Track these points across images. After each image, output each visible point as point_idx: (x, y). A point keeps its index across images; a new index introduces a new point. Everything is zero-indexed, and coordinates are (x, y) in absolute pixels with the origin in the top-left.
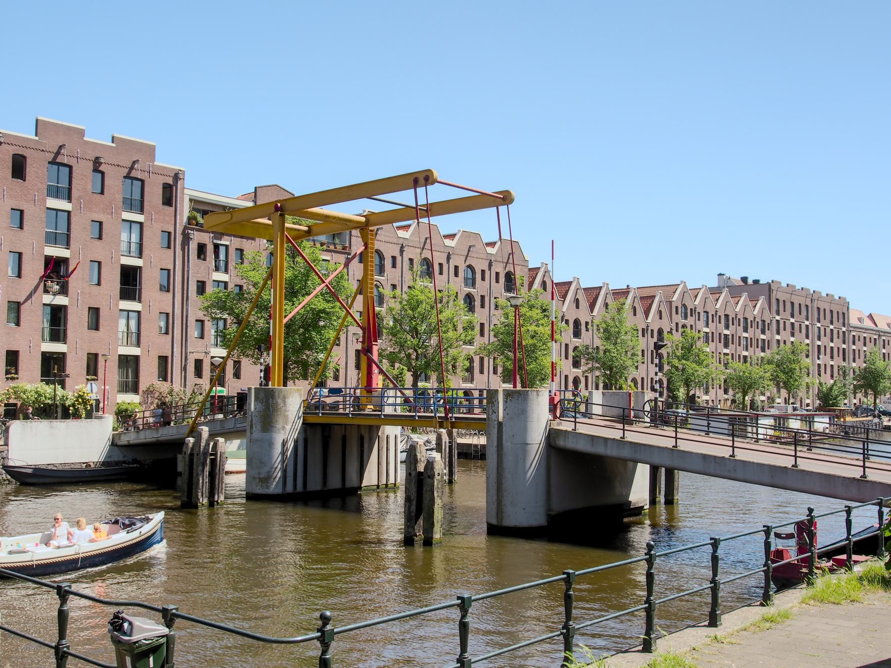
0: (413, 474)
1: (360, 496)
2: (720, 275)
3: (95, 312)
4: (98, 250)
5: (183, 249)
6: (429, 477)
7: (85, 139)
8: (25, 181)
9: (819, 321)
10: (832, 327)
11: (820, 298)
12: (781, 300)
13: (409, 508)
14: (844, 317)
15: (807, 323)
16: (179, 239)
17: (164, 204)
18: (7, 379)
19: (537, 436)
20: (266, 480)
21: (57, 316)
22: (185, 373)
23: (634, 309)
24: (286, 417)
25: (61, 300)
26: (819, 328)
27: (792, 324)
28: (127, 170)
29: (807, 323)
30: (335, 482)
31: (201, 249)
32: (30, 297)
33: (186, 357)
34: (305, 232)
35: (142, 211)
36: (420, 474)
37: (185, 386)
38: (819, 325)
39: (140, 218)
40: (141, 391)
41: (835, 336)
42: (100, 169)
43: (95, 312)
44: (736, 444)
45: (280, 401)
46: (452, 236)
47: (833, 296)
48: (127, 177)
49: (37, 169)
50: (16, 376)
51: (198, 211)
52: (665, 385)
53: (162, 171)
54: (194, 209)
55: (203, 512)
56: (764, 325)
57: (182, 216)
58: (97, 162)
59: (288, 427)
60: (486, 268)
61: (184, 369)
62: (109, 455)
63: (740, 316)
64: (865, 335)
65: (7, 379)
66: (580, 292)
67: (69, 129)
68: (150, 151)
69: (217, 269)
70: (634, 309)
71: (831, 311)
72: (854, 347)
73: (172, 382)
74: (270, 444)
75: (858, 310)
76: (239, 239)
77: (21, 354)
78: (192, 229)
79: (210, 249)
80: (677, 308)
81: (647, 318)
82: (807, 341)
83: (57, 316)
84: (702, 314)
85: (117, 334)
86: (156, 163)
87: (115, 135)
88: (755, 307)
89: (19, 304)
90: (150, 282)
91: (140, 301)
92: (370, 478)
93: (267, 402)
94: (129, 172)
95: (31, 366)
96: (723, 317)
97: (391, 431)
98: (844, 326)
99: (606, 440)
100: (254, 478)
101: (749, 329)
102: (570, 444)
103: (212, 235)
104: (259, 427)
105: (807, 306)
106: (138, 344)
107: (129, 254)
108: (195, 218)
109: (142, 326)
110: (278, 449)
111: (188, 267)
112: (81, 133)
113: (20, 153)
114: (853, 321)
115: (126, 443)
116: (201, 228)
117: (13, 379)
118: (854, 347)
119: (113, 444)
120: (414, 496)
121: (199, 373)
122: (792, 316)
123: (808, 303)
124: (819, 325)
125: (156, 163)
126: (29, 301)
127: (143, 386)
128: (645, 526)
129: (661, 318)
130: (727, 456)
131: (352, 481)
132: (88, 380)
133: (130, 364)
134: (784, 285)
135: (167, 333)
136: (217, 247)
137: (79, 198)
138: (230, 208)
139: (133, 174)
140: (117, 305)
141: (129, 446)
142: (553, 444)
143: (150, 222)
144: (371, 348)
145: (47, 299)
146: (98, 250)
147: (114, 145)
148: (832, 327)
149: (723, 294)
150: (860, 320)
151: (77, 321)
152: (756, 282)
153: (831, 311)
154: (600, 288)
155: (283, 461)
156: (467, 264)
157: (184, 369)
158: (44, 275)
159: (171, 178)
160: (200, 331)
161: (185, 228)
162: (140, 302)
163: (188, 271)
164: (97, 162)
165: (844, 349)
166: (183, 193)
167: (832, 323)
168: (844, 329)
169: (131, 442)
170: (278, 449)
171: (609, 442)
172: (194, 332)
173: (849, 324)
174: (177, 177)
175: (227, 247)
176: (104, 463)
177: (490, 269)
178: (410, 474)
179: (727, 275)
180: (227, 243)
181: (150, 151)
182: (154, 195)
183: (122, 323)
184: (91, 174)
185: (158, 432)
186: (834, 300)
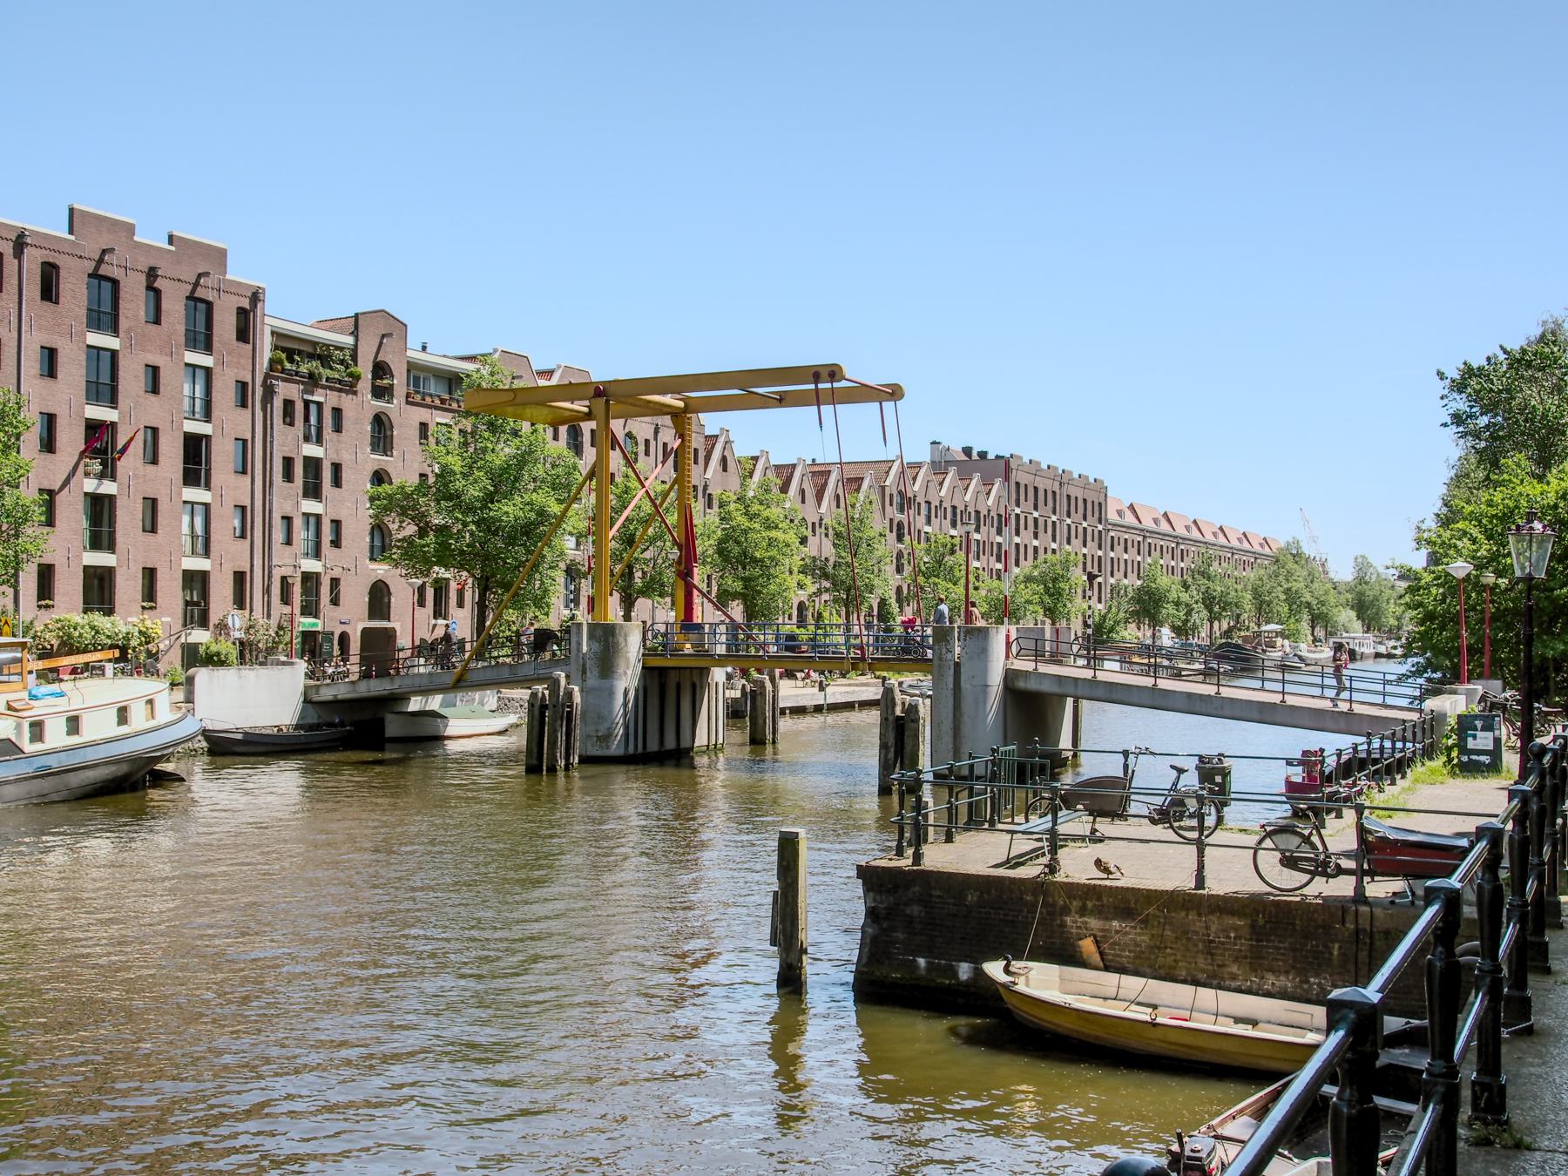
0: (891, 718)
1: (693, 758)
2: (934, 443)
3: (152, 504)
4: (153, 411)
5: (264, 409)
6: (913, 721)
7: (136, 238)
8: (57, 302)
9: (1069, 515)
10: (1085, 524)
11: (1070, 481)
12: (1022, 483)
13: (886, 756)
14: (1099, 509)
15: (1054, 518)
16: (259, 392)
17: (238, 339)
18: (40, 607)
19: (996, 678)
20: (606, 738)
21: (100, 510)
22: (269, 597)
23: (803, 492)
24: (627, 659)
25: (108, 488)
26: (1069, 526)
27: (1036, 520)
28: (190, 287)
29: (1054, 518)
30: (670, 744)
31: (288, 405)
32: (67, 482)
33: (270, 572)
34: (586, 414)
35: (115, 331)
36: (899, 718)
37: (269, 616)
38: (1069, 521)
39: (207, 361)
40: (211, 625)
41: (1089, 538)
42: (156, 285)
43: (152, 504)
44: (1222, 682)
45: (621, 640)
46: (550, 373)
47: (1039, 464)
48: (191, 298)
49: (74, 288)
50: (51, 603)
51: (284, 350)
52: (875, 613)
53: (235, 288)
54: (276, 348)
55: (561, 774)
56: (954, 514)
57: (262, 358)
58: (152, 274)
59: (629, 672)
60: (650, 436)
61: (267, 591)
62: (302, 717)
63: (971, 509)
64: (1126, 536)
65: (40, 607)
66: (771, 475)
67: (115, 223)
68: (220, 256)
69: (307, 439)
70: (803, 492)
71: (1036, 489)
72: (1112, 554)
73: (251, 611)
74: (611, 693)
75: (1119, 497)
76: (336, 393)
77: (57, 568)
78: (277, 378)
79: (299, 407)
80: (891, 495)
81: (819, 505)
82: (1054, 546)
83: (100, 510)
84: (923, 506)
85: (180, 538)
86: (228, 277)
87: (76, 206)
88: (967, 489)
89: (51, 493)
90: (222, 457)
91: (208, 486)
92: (701, 739)
93: (606, 641)
94: (97, 268)
95: (69, 587)
96: (949, 510)
97: (718, 675)
98: (1100, 523)
99: (1076, 679)
100: (589, 736)
101: (982, 528)
102: (1032, 685)
103: (301, 387)
104: (596, 673)
105: (1054, 493)
106: (207, 553)
107: (192, 416)
108: (280, 362)
109: (213, 525)
110: (619, 700)
111: (272, 436)
112: (130, 229)
113: (51, 260)
114: (1112, 516)
115: (331, 698)
116: (290, 377)
117: (47, 607)
118: (1112, 554)
119: (307, 701)
120: (891, 741)
121: (286, 599)
122: (1036, 508)
123: (1056, 488)
124: (1069, 521)
125: (228, 277)
126: (67, 489)
127: (214, 619)
128: (637, 852)
129: (803, 502)
130: (1213, 694)
131: (685, 744)
132: (143, 608)
133: (196, 582)
134: (1026, 460)
135: (243, 536)
136: (307, 403)
137: (128, 331)
138: (324, 345)
139: (103, 271)
140: (180, 494)
141: (335, 704)
142: (1010, 685)
143: (220, 367)
144: (692, 571)
145: (90, 485)
146: (153, 411)
147: (172, 248)
148: (1085, 524)
149: (974, 482)
150: (1120, 513)
151: (128, 518)
152: (983, 455)
153: (1085, 501)
154: (794, 466)
155: (625, 714)
156: (627, 430)
157: (267, 591)
158: (84, 452)
159: (248, 300)
160: (285, 531)
161: (267, 376)
162: (209, 490)
163: (272, 442)
164: (152, 274)
165: (1100, 557)
166: (263, 323)
167: (1085, 518)
168: (1100, 527)
169: (339, 697)
170: (619, 700)
171: (1080, 683)
172: (278, 535)
173: (1106, 520)
174: (256, 297)
175: (319, 405)
176: (297, 727)
177: (656, 439)
178: (886, 719)
179: (945, 443)
180: (321, 399)
181: (220, 256)
182: (225, 325)
183: (186, 519)
184: (144, 295)
185: (392, 683)
186: (1042, 470)
